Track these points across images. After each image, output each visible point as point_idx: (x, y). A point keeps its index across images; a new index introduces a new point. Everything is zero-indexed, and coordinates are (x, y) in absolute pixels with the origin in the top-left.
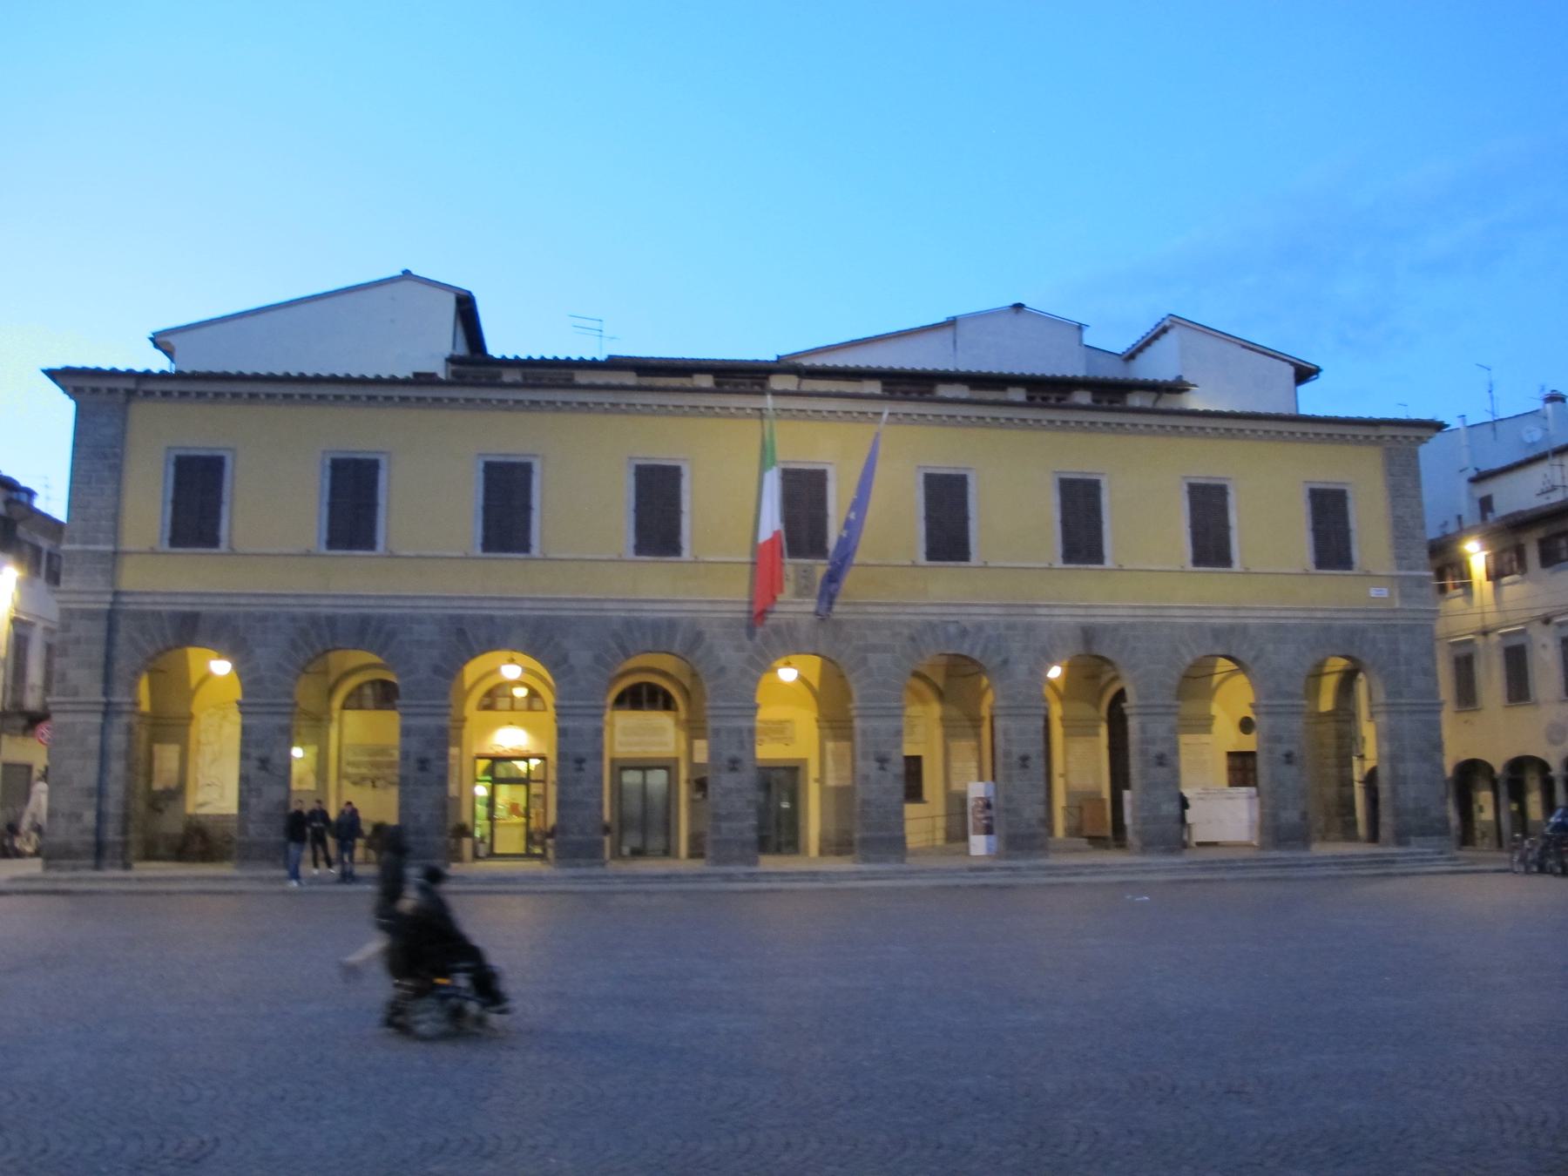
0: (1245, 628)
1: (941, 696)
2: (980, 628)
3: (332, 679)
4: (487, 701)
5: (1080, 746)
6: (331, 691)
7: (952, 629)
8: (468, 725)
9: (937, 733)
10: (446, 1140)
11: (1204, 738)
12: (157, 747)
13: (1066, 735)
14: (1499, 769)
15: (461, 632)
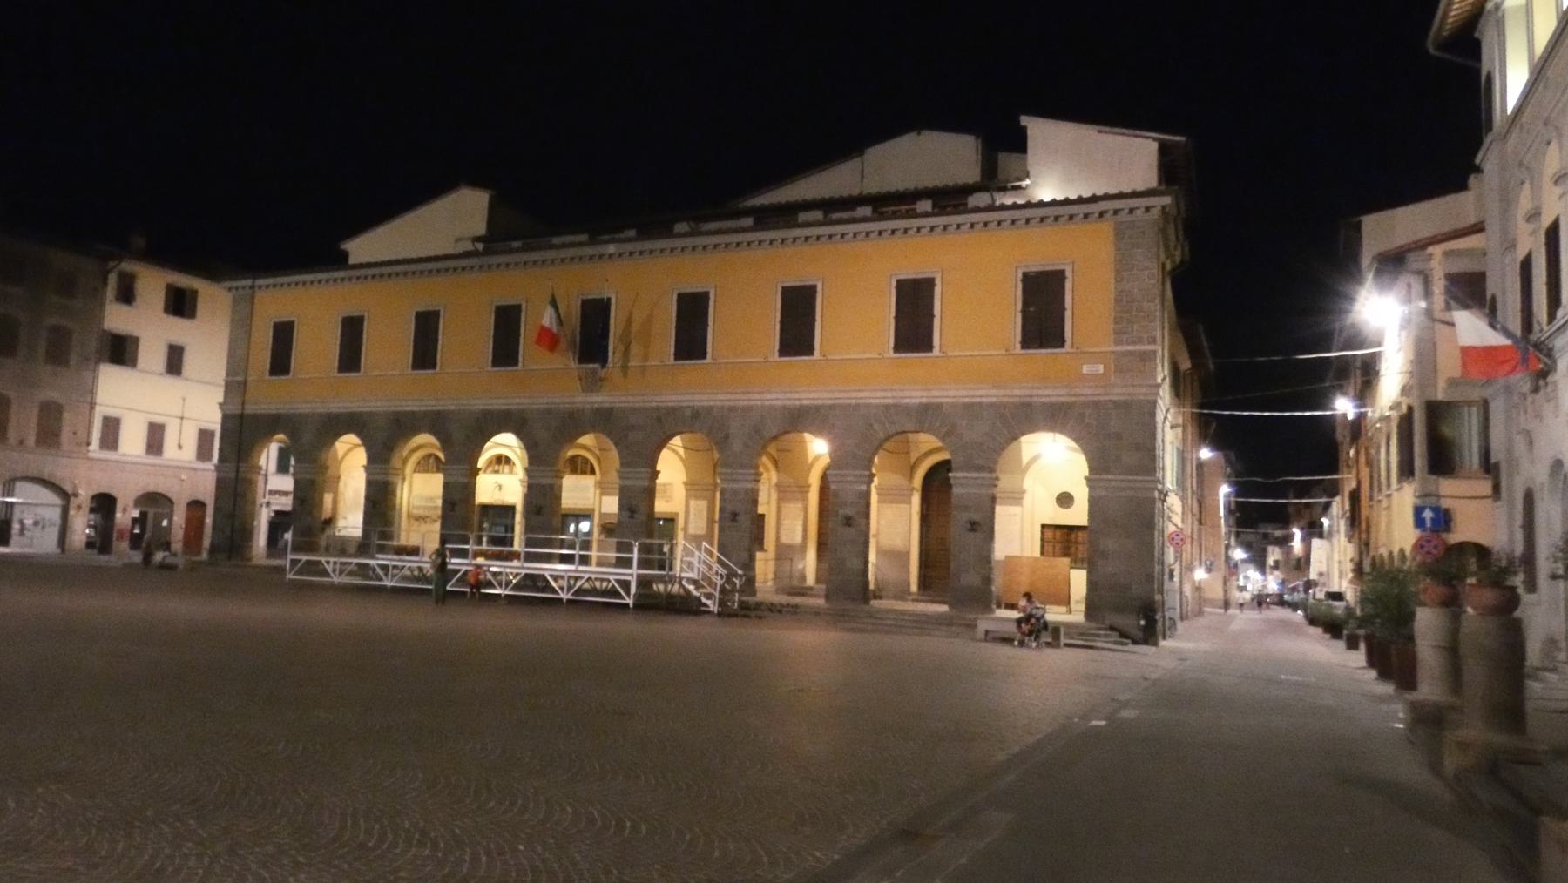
0: (940, 406)
2: (709, 410)
9: (774, 496)
13: (879, 502)
15: (659, 420)
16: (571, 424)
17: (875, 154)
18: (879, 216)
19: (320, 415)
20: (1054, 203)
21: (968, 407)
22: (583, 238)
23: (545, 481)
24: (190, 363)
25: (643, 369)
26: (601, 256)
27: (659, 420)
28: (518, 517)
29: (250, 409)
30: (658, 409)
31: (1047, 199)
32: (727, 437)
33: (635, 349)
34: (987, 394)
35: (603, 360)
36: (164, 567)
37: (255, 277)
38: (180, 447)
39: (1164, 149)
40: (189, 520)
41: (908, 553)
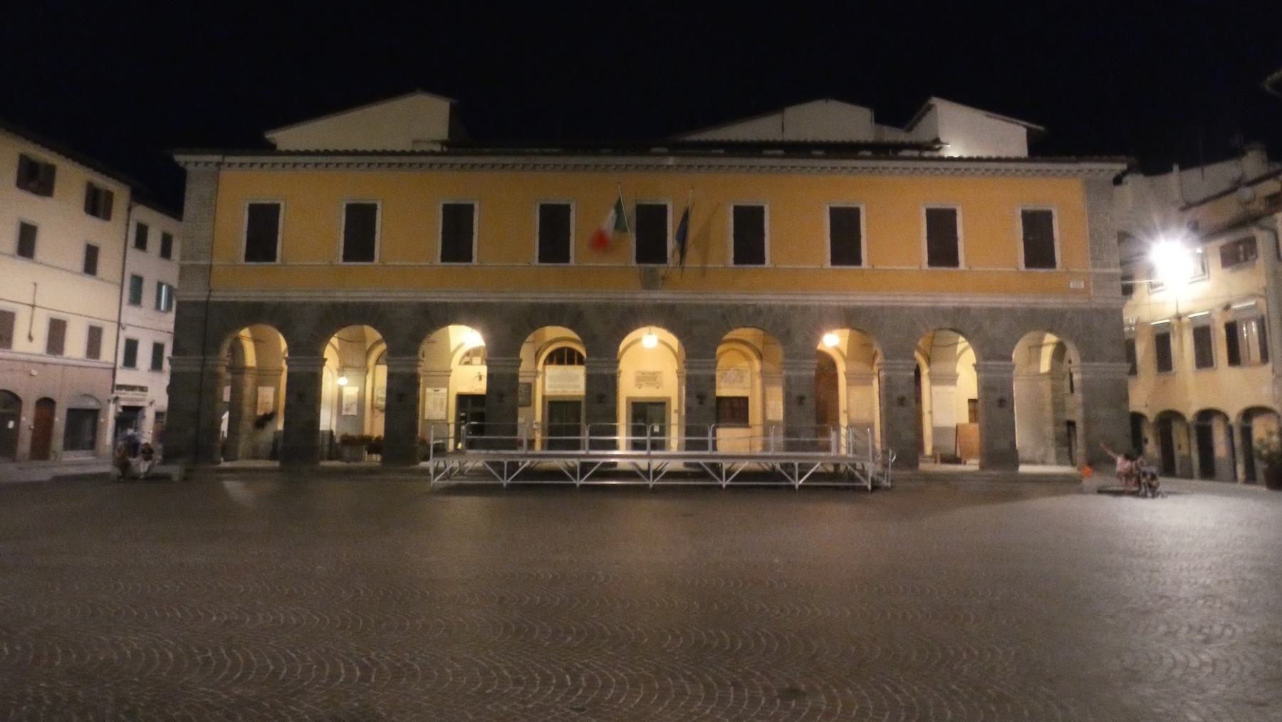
0: (968, 310)
1: (760, 357)
2: (771, 308)
3: (368, 345)
4: (467, 359)
5: (858, 393)
6: (368, 353)
7: (751, 310)
8: (453, 374)
9: (758, 382)
10: (531, 443)
11: (950, 389)
12: (260, 389)
13: (848, 384)
14: (1234, 417)
15: (724, 317)
16: (730, 317)
17: (792, 113)
18: (876, 157)
19: (321, 305)
20: (960, 159)
21: (990, 310)
22: (665, 150)
23: (606, 371)
24: (43, 243)
25: (703, 271)
26: (658, 166)
27: (724, 317)
28: (583, 406)
29: (218, 296)
30: (721, 306)
31: (956, 155)
32: (788, 332)
33: (691, 252)
34: (1003, 301)
35: (662, 258)
36: (151, 478)
37: (226, 154)
38: (30, 338)
39: (1030, 134)
40: (37, 421)
41: (871, 425)
